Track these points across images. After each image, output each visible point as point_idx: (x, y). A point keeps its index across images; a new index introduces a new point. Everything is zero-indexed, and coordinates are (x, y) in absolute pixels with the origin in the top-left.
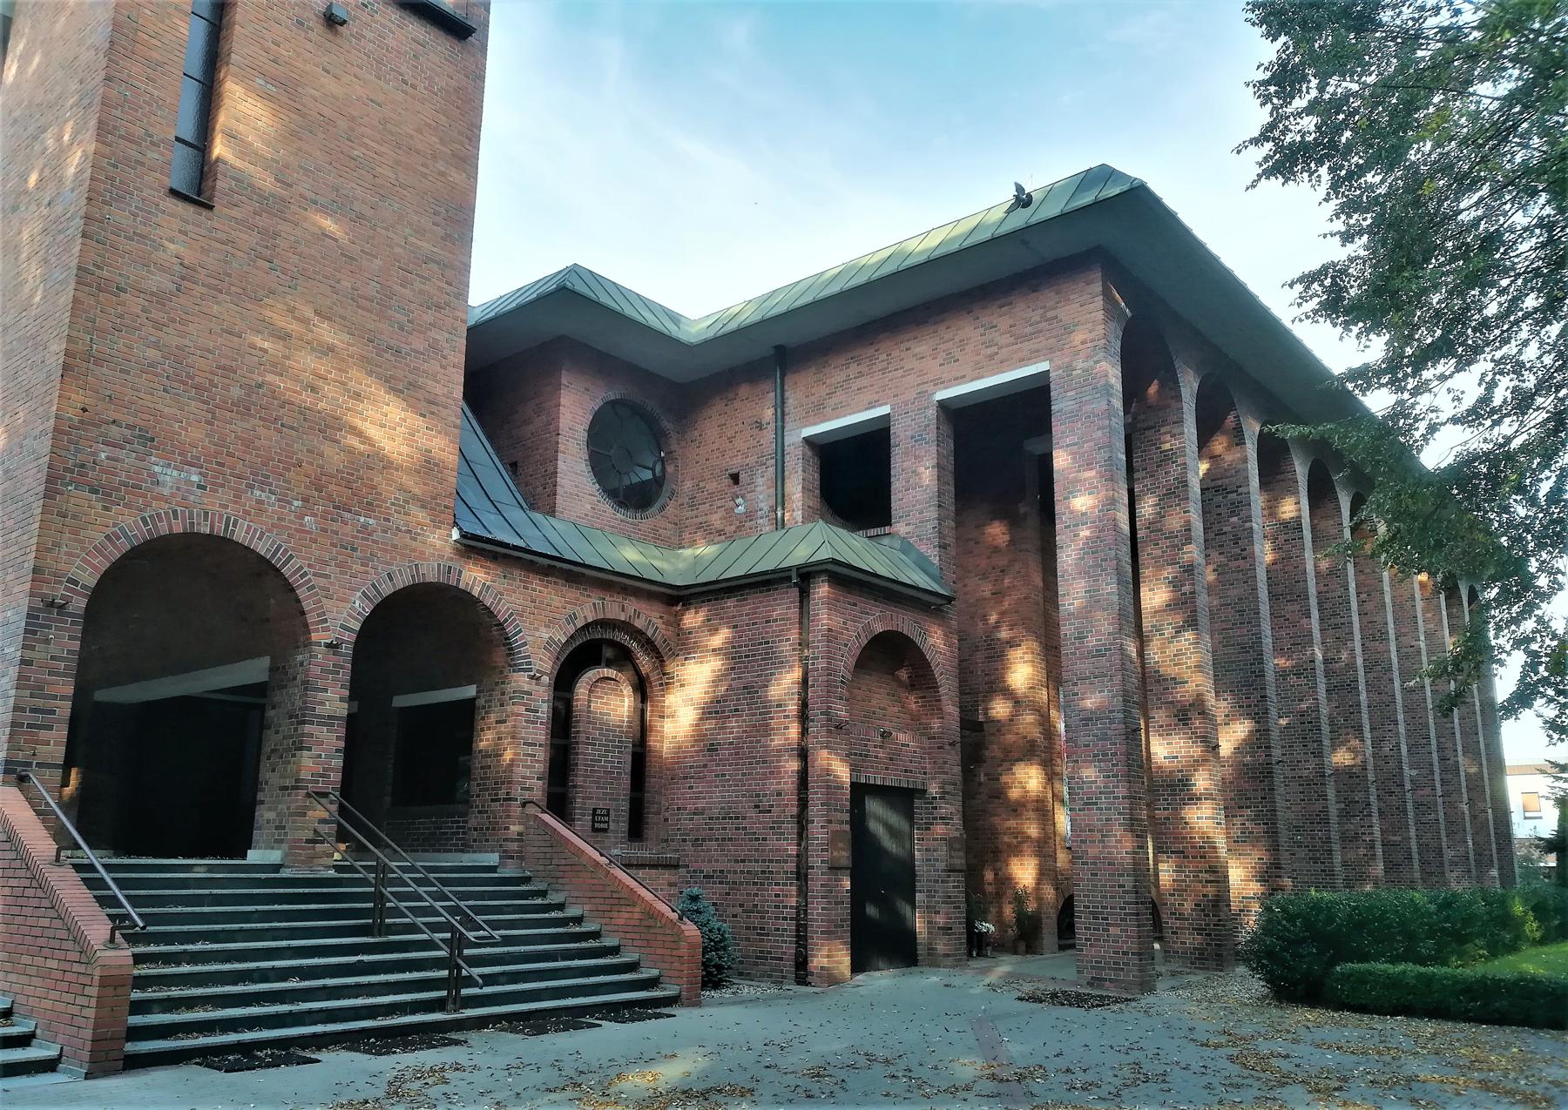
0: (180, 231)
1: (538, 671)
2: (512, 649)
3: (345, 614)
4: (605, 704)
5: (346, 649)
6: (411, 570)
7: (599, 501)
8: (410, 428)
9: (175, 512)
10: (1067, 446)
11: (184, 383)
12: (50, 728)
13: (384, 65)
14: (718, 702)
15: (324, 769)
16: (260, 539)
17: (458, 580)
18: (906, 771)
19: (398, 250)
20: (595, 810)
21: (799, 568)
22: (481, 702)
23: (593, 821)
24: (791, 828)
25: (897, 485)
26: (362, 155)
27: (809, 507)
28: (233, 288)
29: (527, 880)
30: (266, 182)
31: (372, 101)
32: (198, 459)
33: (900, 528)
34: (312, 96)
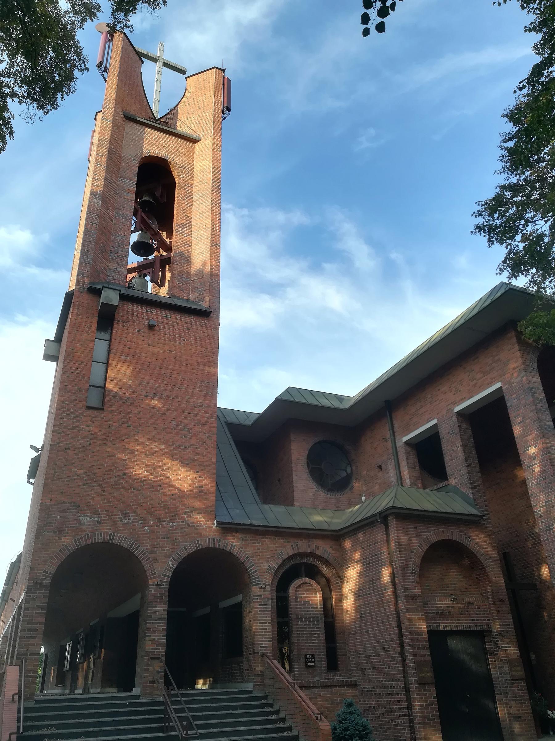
0: (91, 421)
1: (264, 584)
2: (249, 575)
3: (164, 569)
4: (306, 597)
5: (166, 586)
6: (195, 543)
7: (316, 491)
8: (193, 479)
9: (88, 535)
10: (519, 423)
11: (92, 481)
12: (35, 638)
13: (174, 336)
14: (361, 590)
15: (157, 646)
16: (125, 540)
17: (219, 545)
18: (474, 620)
19: (183, 405)
20: (306, 655)
21: (380, 513)
22: (244, 603)
23: (306, 662)
24: (399, 661)
25: (447, 459)
26: (166, 373)
27: (413, 476)
28: (112, 438)
29: (265, 698)
30: (128, 394)
31: (169, 351)
32: (98, 511)
33: (452, 481)
34: (144, 356)
